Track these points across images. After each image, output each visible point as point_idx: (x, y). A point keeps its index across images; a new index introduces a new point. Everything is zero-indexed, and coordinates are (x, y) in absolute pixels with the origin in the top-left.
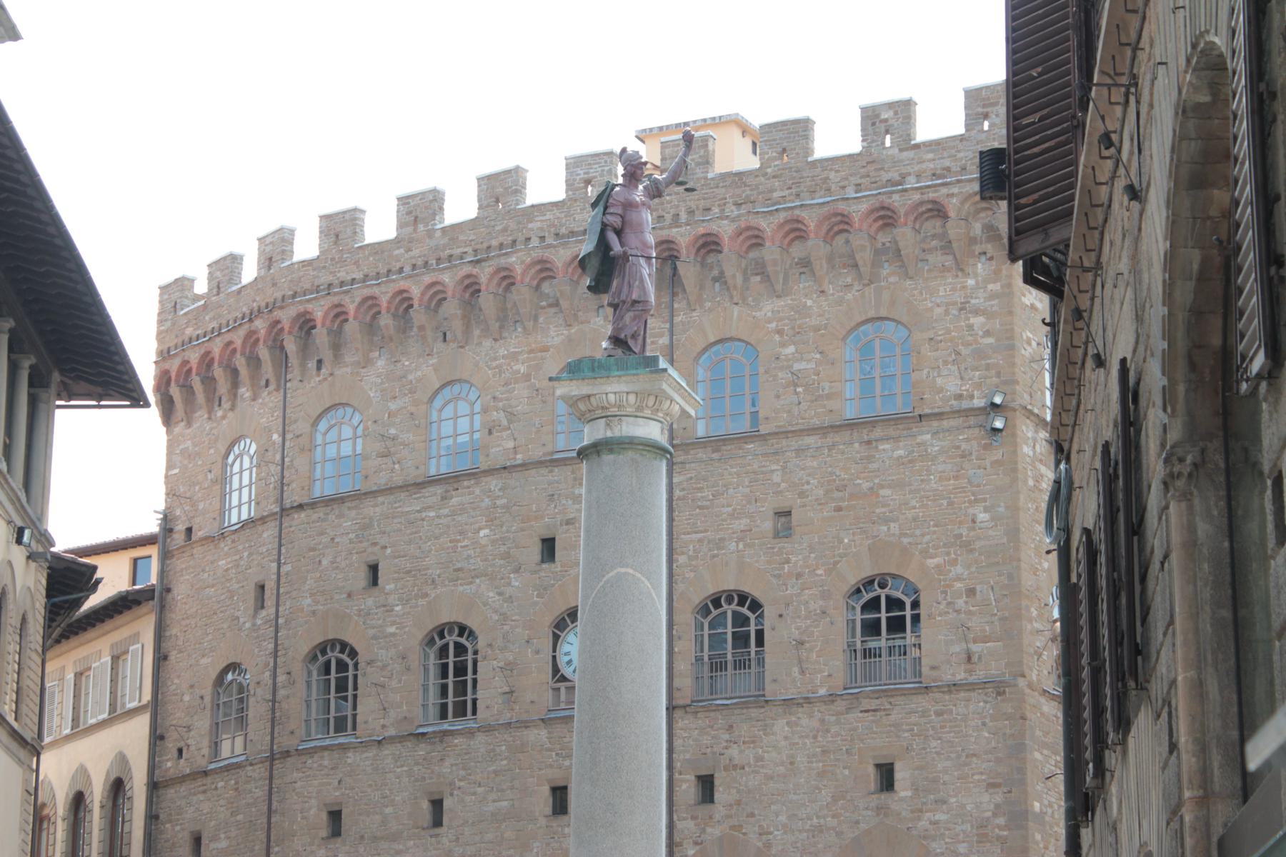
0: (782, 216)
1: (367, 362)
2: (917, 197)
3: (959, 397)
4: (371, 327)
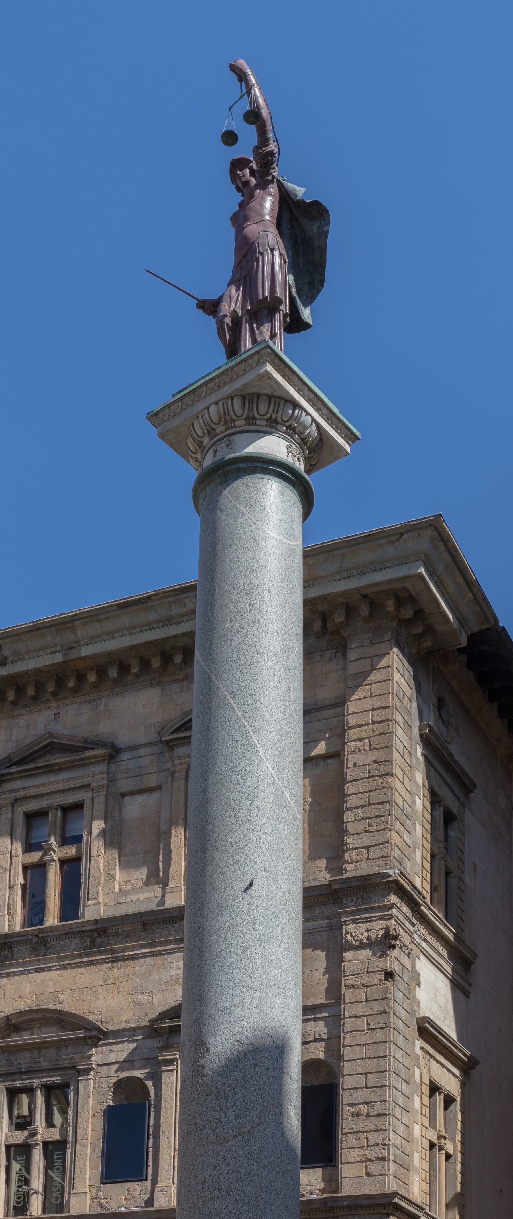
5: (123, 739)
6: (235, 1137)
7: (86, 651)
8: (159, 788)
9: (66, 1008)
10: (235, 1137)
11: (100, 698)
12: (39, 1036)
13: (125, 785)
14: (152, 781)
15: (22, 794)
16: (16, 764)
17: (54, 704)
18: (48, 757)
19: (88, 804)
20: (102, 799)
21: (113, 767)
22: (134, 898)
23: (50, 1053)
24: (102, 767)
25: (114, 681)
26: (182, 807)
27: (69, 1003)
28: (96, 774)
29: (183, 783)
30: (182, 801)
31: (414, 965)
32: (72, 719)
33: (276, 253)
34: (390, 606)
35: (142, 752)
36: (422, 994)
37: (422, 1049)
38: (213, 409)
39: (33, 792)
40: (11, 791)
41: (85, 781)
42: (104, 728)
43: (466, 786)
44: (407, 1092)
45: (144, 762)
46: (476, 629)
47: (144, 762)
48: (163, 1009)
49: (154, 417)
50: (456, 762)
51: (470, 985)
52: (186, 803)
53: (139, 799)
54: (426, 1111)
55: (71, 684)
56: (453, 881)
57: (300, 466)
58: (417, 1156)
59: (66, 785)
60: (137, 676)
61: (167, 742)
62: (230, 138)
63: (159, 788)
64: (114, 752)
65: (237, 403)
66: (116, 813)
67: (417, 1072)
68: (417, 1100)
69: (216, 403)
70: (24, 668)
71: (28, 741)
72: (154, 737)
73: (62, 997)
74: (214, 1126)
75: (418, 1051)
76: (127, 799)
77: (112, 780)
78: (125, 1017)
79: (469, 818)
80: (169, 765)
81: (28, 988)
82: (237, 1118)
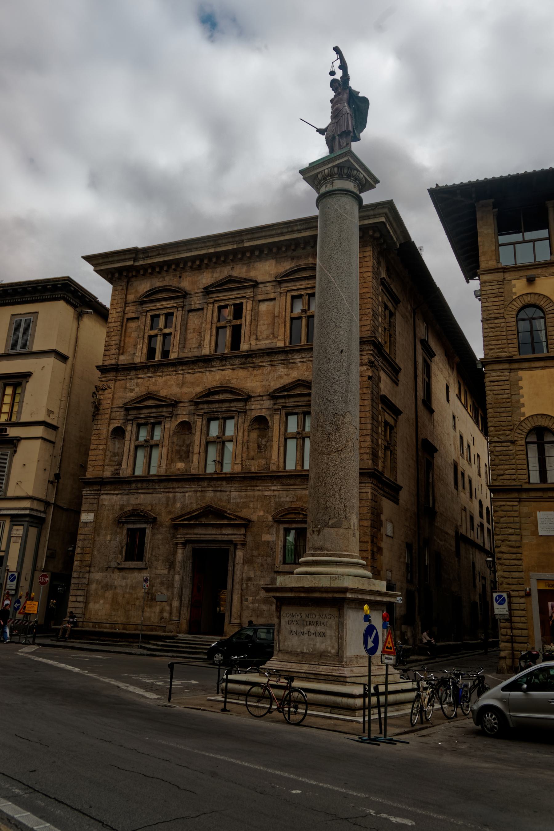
5: (260, 279)
6: (335, 452)
7: (247, 244)
8: (274, 299)
9: (234, 386)
10: (335, 452)
11: (251, 262)
12: (222, 397)
13: (260, 297)
14: (272, 296)
15: (217, 299)
16: (216, 287)
17: (232, 264)
18: (229, 285)
19: (244, 304)
20: (251, 302)
21: (256, 290)
22: (264, 342)
23: (227, 405)
24: (251, 290)
25: (258, 256)
26: (284, 307)
27: (234, 383)
28: (249, 293)
29: (285, 297)
30: (284, 304)
31: (379, 374)
32: (239, 271)
33: (349, 115)
34: (371, 233)
35: (268, 284)
36: (382, 386)
37: (382, 408)
38: (326, 171)
39: (222, 298)
40: (213, 298)
41: (244, 295)
42: (252, 274)
43: (396, 301)
44: (377, 426)
45: (269, 288)
46: (403, 242)
47: (269, 288)
48: (275, 388)
49: (302, 172)
50: (394, 292)
51: (399, 381)
52: (286, 305)
53: (266, 303)
54: (383, 433)
55: (239, 256)
56: (392, 339)
57: (356, 191)
58: (380, 452)
59: (236, 296)
60: (267, 255)
61: (278, 281)
62: (332, 73)
63: (274, 299)
64: (255, 284)
65: (336, 169)
66: (257, 308)
67: (380, 417)
68: (380, 428)
69: (328, 169)
70: (221, 250)
71: (221, 278)
72: (273, 279)
73: (232, 382)
74: (327, 447)
75: (380, 408)
76: (261, 303)
77: (255, 295)
78: (259, 391)
79: (398, 314)
80: (279, 290)
81: (217, 377)
82: (336, 444)
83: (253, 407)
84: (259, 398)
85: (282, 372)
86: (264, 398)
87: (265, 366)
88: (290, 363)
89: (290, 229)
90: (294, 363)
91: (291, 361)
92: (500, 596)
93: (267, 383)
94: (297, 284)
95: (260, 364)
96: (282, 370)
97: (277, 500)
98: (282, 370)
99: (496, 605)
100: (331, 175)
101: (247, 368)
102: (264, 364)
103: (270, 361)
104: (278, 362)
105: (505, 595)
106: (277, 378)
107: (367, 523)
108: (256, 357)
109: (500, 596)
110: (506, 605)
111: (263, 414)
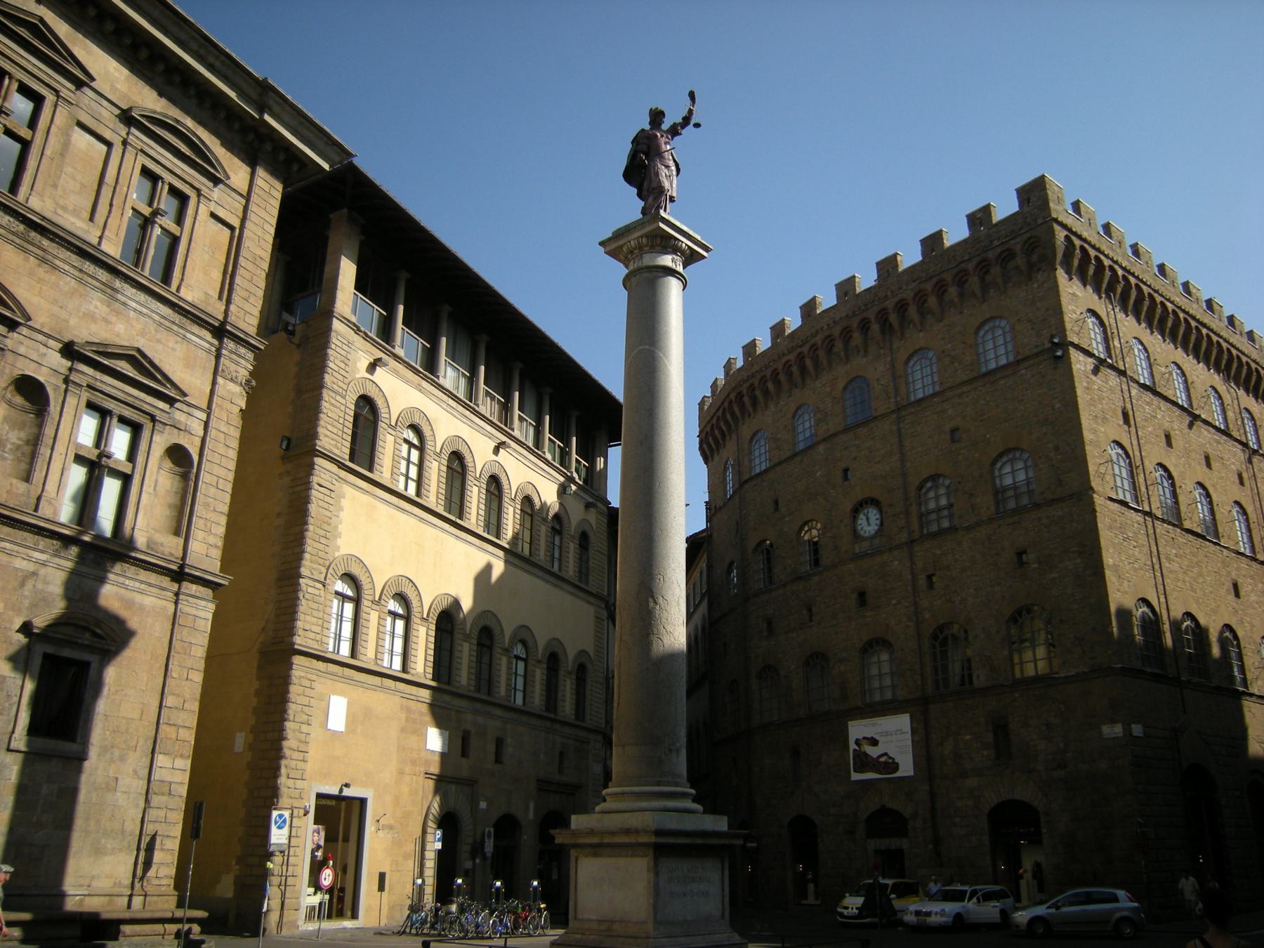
0: (935, 280)
1: (767, 407)
2: (999, 250)
3: (1037, 346)
4: (766, 393)
45: (105, 114)
83: (22, 350)
84: (40, 337)
85: (96, 307)
86: (51, 343)
87: (65, 273)
88: (117, 300)
89: (202, 52)
90: (124, 304)
91: (119, 296)
92: (281, 816)
93: (63, 315)
94: (176, 161)
95: (57, 262)
96: (96, 303)
97: (40, 586)
98: (99, 304)
99: (274, 829)
100: (640, 248)
101: (25, 251)
102: (67, 267)
103: (81, 271)
104: (94, 282)
105: (287, 814)
106: (84, 314)
107: (473, 671)
108: (51, 240)
109: (281, 816)
110: (286, 830)
111: (41, 379)
